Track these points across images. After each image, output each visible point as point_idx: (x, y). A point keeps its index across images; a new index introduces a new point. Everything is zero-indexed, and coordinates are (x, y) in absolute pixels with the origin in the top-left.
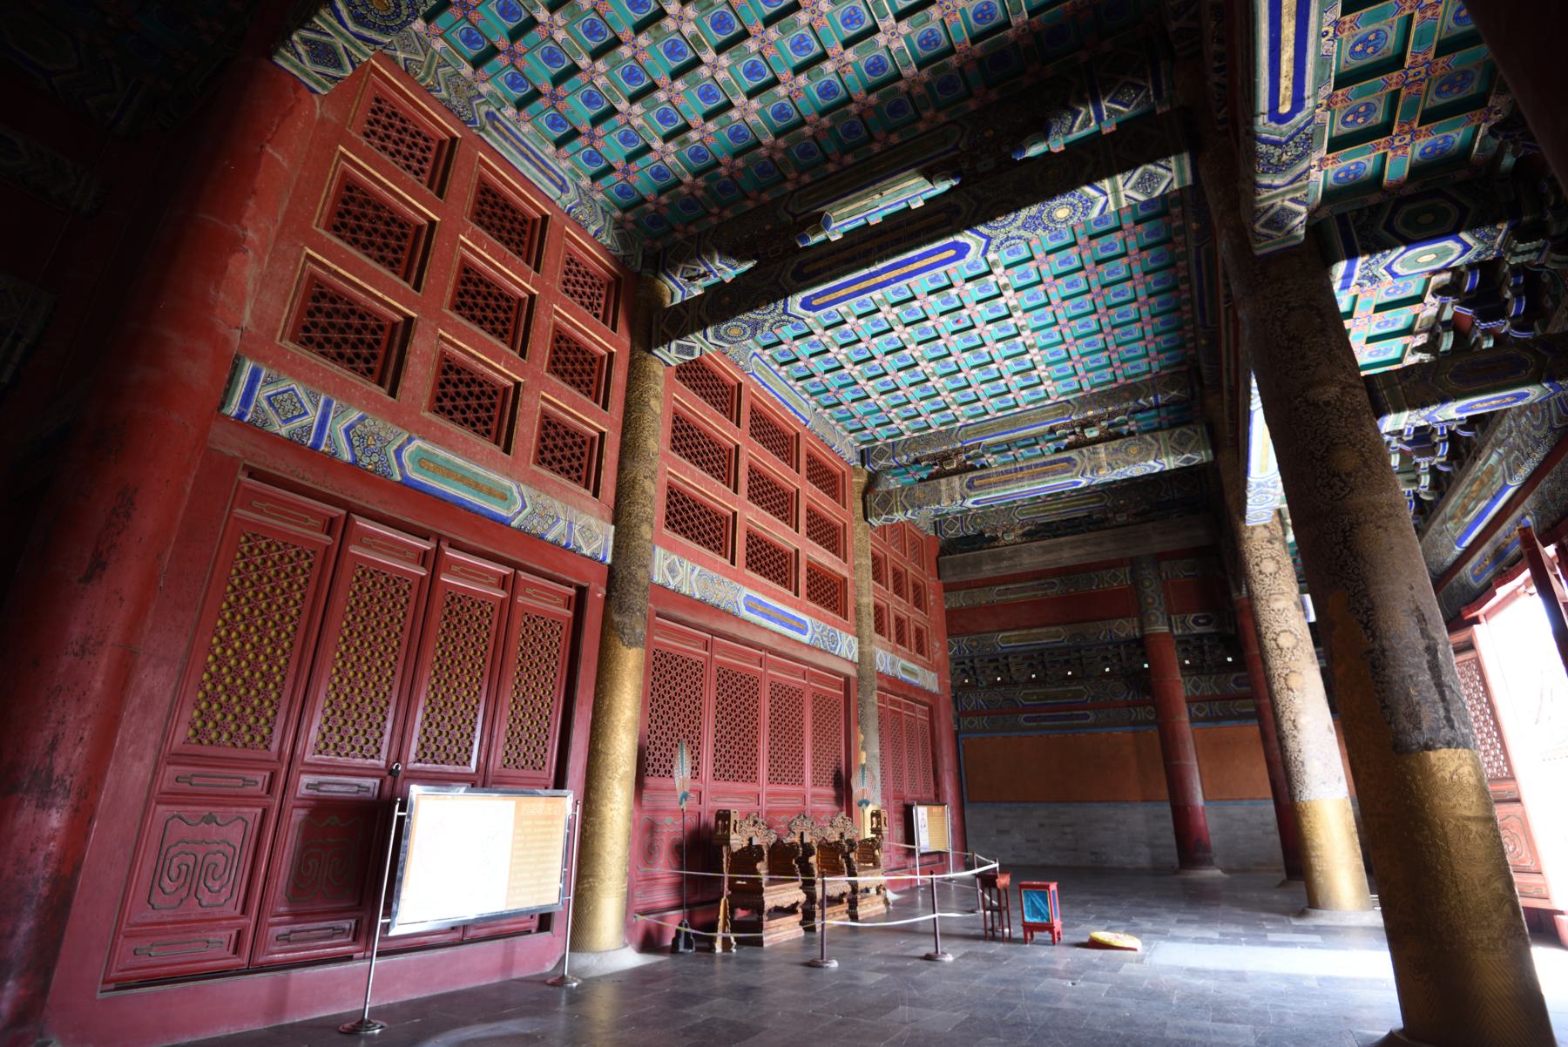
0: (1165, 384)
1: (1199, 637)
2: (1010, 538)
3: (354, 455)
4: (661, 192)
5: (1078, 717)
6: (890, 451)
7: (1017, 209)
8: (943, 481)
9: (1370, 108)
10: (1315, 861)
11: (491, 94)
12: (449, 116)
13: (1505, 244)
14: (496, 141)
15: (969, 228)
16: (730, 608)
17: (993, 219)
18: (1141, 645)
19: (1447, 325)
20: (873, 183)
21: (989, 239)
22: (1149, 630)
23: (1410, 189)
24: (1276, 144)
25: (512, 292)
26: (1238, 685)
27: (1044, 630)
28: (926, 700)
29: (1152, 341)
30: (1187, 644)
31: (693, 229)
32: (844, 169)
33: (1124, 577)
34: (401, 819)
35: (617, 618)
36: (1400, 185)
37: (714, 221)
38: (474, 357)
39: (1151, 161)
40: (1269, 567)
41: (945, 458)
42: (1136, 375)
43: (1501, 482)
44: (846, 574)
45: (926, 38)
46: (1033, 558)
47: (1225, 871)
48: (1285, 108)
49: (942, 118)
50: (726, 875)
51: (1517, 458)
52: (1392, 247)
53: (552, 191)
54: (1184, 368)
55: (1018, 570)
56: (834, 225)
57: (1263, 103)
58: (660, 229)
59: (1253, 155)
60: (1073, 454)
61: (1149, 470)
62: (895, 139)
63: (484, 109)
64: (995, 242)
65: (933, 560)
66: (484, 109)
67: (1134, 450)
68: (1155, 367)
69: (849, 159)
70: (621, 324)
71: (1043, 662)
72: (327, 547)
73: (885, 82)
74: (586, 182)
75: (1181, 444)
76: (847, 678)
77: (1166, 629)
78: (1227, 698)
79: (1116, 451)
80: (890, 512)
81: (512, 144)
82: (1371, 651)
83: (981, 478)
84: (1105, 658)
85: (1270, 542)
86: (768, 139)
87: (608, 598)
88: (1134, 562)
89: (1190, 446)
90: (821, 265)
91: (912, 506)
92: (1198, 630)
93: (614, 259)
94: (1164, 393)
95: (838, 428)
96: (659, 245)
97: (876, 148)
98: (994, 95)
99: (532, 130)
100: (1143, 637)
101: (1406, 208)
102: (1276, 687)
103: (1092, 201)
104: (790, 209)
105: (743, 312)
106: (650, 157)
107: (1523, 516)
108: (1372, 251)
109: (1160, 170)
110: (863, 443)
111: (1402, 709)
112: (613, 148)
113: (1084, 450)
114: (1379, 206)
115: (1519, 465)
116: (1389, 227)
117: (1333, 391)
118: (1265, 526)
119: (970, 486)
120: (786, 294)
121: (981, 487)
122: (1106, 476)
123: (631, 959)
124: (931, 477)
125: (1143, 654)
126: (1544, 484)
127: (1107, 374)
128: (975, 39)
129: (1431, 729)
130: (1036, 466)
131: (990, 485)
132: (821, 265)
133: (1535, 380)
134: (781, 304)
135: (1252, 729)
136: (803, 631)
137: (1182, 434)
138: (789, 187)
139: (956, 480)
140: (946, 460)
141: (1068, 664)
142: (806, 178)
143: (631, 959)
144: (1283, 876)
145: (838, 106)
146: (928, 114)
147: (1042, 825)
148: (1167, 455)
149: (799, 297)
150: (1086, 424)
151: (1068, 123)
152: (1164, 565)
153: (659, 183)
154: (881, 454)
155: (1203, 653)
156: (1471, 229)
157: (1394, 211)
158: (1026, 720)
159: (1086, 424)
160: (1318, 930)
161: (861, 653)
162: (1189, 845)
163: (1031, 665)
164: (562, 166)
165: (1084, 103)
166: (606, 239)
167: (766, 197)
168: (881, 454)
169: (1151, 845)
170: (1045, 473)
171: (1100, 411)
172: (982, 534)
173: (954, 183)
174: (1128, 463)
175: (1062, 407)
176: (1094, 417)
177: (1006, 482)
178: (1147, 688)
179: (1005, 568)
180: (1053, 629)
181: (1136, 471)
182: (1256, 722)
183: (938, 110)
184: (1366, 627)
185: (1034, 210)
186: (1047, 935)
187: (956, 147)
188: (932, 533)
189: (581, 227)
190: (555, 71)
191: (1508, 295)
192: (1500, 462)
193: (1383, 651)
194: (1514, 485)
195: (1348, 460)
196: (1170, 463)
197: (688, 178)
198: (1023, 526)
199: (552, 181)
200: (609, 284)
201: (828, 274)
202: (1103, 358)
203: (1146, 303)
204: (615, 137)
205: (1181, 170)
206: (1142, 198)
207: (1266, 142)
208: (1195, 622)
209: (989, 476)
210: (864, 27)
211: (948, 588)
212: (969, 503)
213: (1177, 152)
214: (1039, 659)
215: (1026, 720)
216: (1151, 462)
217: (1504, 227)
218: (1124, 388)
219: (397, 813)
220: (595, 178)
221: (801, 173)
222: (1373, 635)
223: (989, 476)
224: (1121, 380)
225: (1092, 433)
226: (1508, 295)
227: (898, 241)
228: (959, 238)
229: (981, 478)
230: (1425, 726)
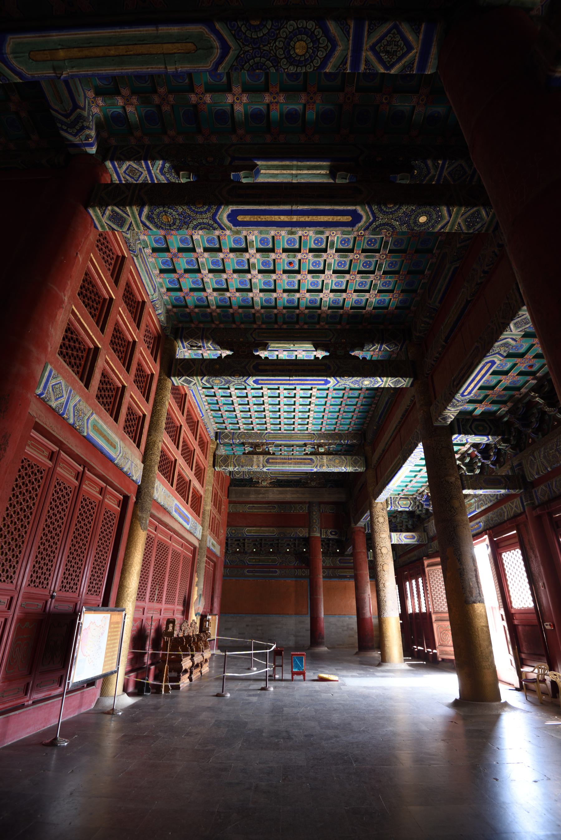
0: (352, 437)
1: (329, 540)
2: (264, 484)
3: (74, 421)
4: (196, 307)
5: (272, 572)
6: (231, 436)
7: (353, 376)
8: (255, 456)
9: (479, 395)
10: (386, 643)
11: (144, 241)
12: (125, 245)
13: (498, 442)
14: (139, 263)
15: (334, 376)
16: (169, 509)
17: (343, 377)
18: (307, 541)
19: (469, 455)
20: (293, 341)
21: (338, 382)
22: (313, 534)
23: (478, 418)
24: (458, 401)
25: (127, 337)
26: (340, 563)
27: (267, 529)
28: (215, 559)
29: (354, 420)
30: (326, 543)
31: (202, 325)
32: (281, 329)
33: (304, 510)
34: (79, 623)
35: (140, 514)
36: (476, 416)
37: (214, 326)
38: (113, 370)
39: (402, 377)
40: (381, 520)
41: (257, 445)
42: (342, 430)
43: (474, 509)
44: (202, 494)
45: (336, 300)
46: (274, 495)
47: (328, 648)
48: (465, 394)
49: (327, 327)
50: (168, 652)
51: (482, 503)
52: (471, 434)
53: (150, 290)
54: (360, 432)
55: (267, 499)
56: (269, 349)
57: (461, 391)
58: (187, 321)
59: (451, 401)
60: (313, 457)
61: (341, 471)
62: (306, 326)
63: (139, 246)
64: (340, 384)
65: (227, 488)
66: (139, 246)
67: (337, 461)
68: (351, 429)
69: (285, 326)
70: (158, 360)
71: (261, 544)
72: (49, 468)
73: (314, 308)
74: (164, 290)
75: (355, 463)
76: (195, 548)
77: (319, 535)
78: (335, 568)
79: (330, 460)
80: (227, 466)
81: (144, 266)
82: (460, 569)
83: (273, 459)
84: (288, 545)
85: (382, 510)
86: (258, 308)
87: (136, 503)
88: (310, 504)
89: (358, 465)
90: (268, 368)
91: (239, 465)
92: (331, 537)
93: (161, 326)
94: (351, 440)
95: (212, 420)
96: (180, 325)
97: (297, 327)
98: (348, 327)
99: (154, 262)
100: (309, 537)
101: (476, 423)
102: (379, 569)
103: (378, 382)
104: (254, 335)
105: (227, 376)
106: (202, 294)
107: (480, 522)
108: (465, 434)
109: (403, 381)
110: (219, 429)
111: (468, 589)
112: (187, 282)
113: (318, 457)
114: (469, 419)
115: (482, 506)
116: (471, 427)
117: (453, 479)
118: (381, 503)
119: (267, 461)
120: (249, 375)
121: (272, 463)
122: (325, 469)
123: (128, 701)
124: (249, 453)
125: (305, 545)
126: (490, 514)
127: (332, 427)
128: (352, 308)
129: (475, 596)
130: (298, 459)
131: (276, 463)
132: (268, 368)
133: (504, 488)
134: (245, 378)
135: (352, 583)
136: (188, 523)
137: (356, 459)
138: (255, 326)
139: (261, 457)
140: (257, 449)
141: (272, 546)
142: (264, 326)
143: (128, 701)
144: (357, 650)
145: (293, 308)
146: (322, 324)
147: (247, 626)
148: (349, 467)
149: (254, 378)
150: (320, 445)
151: (370, 347)
152: (322, 506)
153: (198, 303)
154: (227, 436)
155: (329, 547)
156: (492, 435)
157: (473, 423)
158: (248, 572)
159: (320, 445)
160: (388, 671)
161: (203, 535)
162: (316, 635)
163: (255, 544)
164: (158, 280)
165: (378, 343)
166: (162, 318)
167: (243, 326)
168: (227, 436)
169: (296, 636)
170: (301, 463)
171: (326, 441)
172: (252, 479)
173: (328, 354)
174: (335, 466)
175: (311, 435)
176: (323, 443)
177: (284, 463)
178: (306, 561)
179: (260, 498)
180: (272, 529)
181: (336, 470)
182: (353, 580)
183: (327, 323)
184: (459, 561)
185: (359, 379)
186: (301, 677)
187: (330, 340)
188: (228, 475)
189: (155, 309)
190: (182, 246)
191: (492, 454)
192: (475, 502)
193: (464, 569)
194: (478, 511)
195: (456, 504)
196: (349, 469)
197: (214, 307)
198: (271, 479)
199: (152, 286)
200: (155, 337)
201: (271, 373)
202: (334, 421)
203: (359, 407)
204: (191, 280)
205: (408, 382)
206: (393, 386)
207: (456, 399)
208: (331, 533)
209: (276, 459)
210: (317, 288)
211: (230, 502)
212: (265, 470)
213: (410, 377)
214: (259, 542)
215: (248, 572)
216: (343, 468)
217: (500, 437)
218: (337, 434)
219: (78, 621)
220: (169, 290)
221: (263, 323)
222: (461, 564)
223: (276, 459)
224: (337, 431)
225: (322, 450)
226: (492, 454)
227: (304, 371)
228: (329, 379)
229: (273, 459)
230: (474, 595)
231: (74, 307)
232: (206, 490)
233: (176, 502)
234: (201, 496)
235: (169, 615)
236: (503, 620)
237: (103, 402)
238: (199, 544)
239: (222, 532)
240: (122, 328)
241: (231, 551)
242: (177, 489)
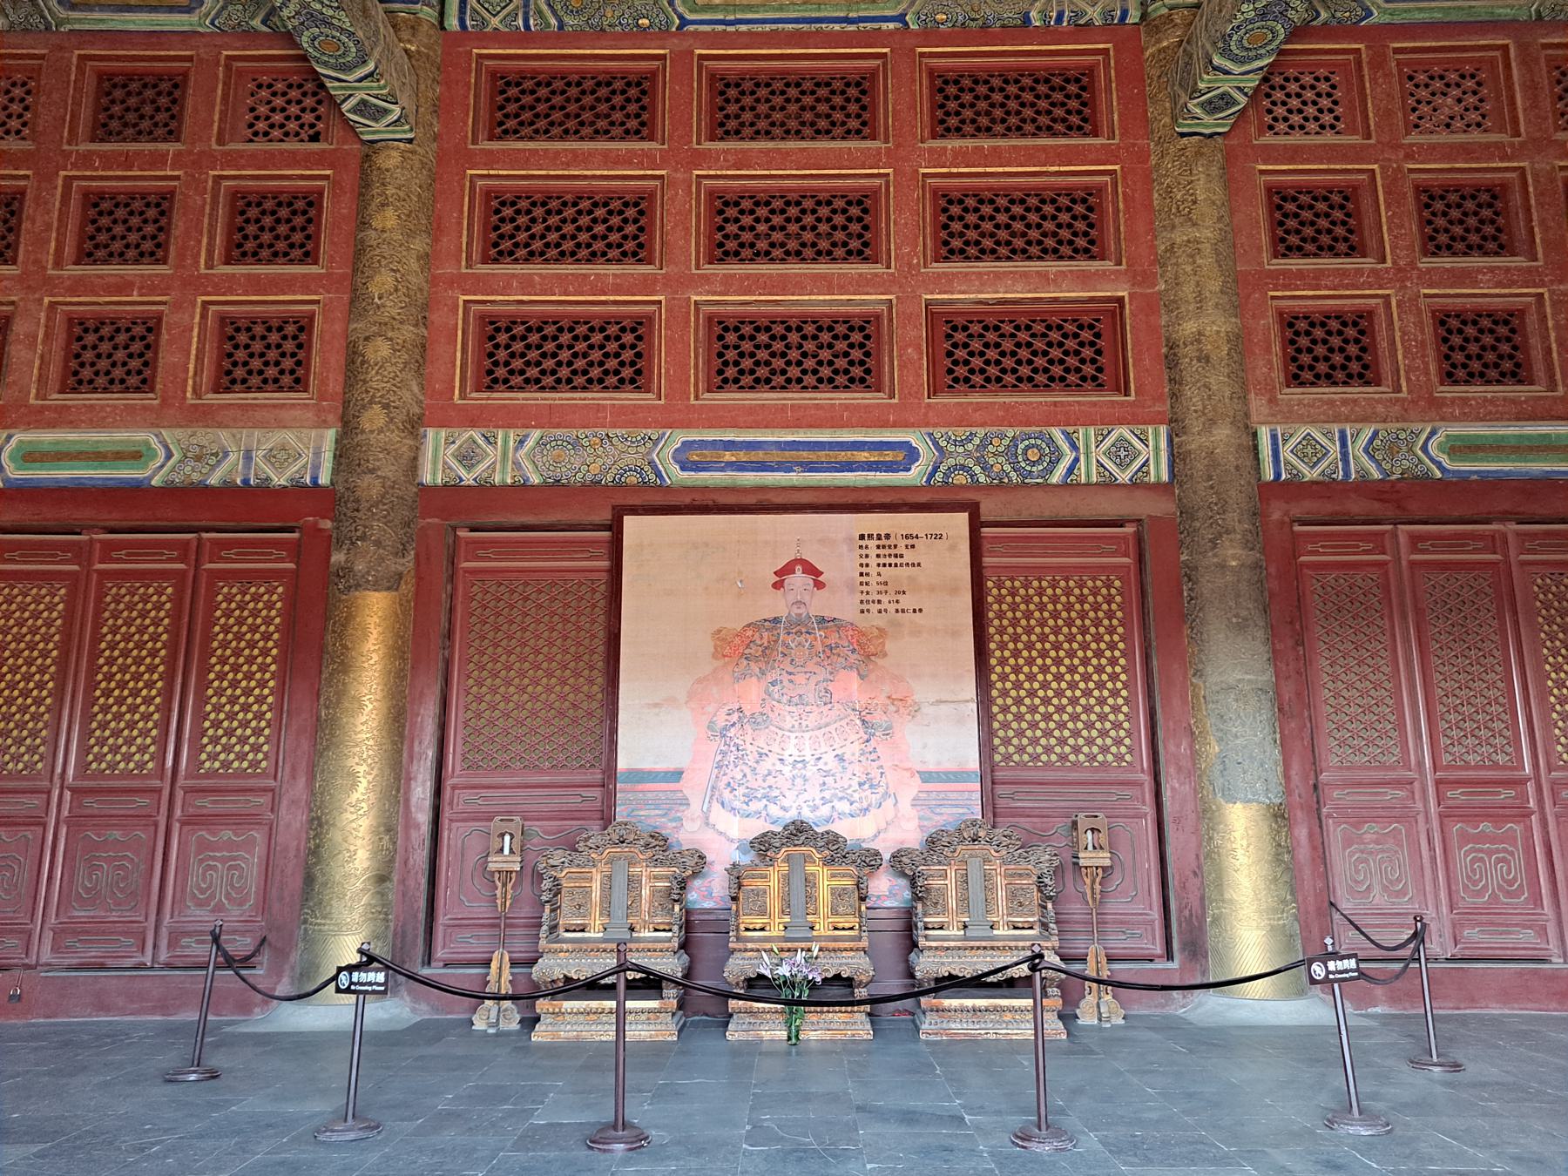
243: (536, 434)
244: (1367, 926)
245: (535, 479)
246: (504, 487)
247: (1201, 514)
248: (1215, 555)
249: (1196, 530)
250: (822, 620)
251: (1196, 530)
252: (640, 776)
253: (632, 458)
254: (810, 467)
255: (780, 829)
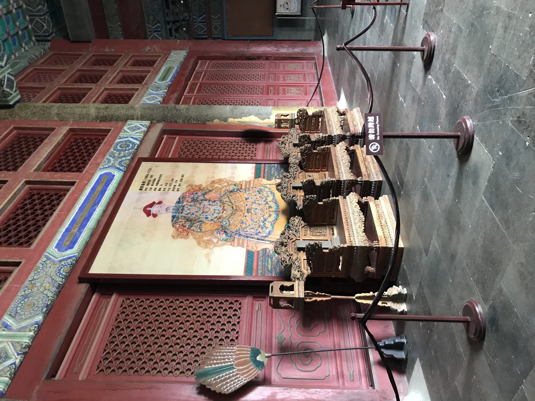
28: (192, 61)
76: (163, 132)
96: (34, 38)
136: (111, 177)
231: (32, 171)
232: (62, 121)
233: (52, 249)
234: (71, 130)
235: (274, 188)
236: (272, 287)
237: (35, 230)
238: (159, 121)
239: (148, 48)
240: (15, 137)
241: (186, 14)
242: (141, 83)
243: (147, 24)
244: (320, 88)
245: (39, 318)
246: (34, 338)
247: (166, 113)
248: (183, 110)
249: (172, 115)
250: (178, 202)
251: (172, 115)
252: (248, 268)
253: (52, 270)
254: (97, 203)
255: (270, 247)
